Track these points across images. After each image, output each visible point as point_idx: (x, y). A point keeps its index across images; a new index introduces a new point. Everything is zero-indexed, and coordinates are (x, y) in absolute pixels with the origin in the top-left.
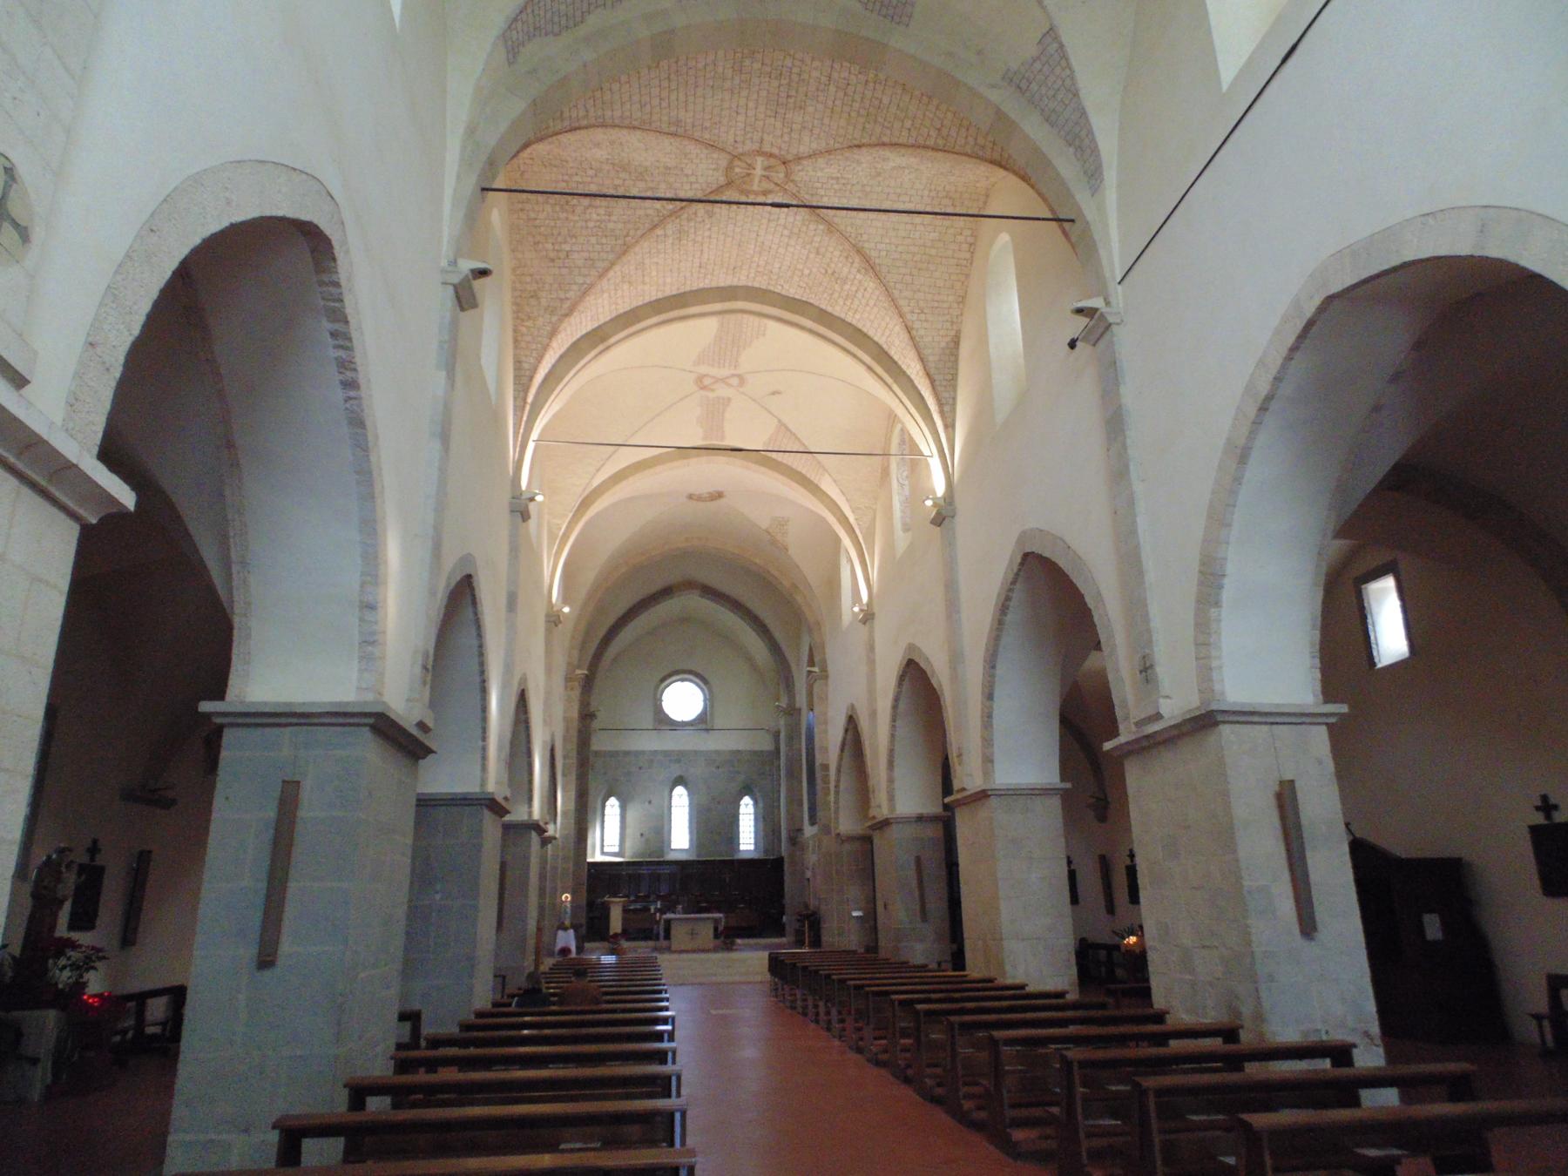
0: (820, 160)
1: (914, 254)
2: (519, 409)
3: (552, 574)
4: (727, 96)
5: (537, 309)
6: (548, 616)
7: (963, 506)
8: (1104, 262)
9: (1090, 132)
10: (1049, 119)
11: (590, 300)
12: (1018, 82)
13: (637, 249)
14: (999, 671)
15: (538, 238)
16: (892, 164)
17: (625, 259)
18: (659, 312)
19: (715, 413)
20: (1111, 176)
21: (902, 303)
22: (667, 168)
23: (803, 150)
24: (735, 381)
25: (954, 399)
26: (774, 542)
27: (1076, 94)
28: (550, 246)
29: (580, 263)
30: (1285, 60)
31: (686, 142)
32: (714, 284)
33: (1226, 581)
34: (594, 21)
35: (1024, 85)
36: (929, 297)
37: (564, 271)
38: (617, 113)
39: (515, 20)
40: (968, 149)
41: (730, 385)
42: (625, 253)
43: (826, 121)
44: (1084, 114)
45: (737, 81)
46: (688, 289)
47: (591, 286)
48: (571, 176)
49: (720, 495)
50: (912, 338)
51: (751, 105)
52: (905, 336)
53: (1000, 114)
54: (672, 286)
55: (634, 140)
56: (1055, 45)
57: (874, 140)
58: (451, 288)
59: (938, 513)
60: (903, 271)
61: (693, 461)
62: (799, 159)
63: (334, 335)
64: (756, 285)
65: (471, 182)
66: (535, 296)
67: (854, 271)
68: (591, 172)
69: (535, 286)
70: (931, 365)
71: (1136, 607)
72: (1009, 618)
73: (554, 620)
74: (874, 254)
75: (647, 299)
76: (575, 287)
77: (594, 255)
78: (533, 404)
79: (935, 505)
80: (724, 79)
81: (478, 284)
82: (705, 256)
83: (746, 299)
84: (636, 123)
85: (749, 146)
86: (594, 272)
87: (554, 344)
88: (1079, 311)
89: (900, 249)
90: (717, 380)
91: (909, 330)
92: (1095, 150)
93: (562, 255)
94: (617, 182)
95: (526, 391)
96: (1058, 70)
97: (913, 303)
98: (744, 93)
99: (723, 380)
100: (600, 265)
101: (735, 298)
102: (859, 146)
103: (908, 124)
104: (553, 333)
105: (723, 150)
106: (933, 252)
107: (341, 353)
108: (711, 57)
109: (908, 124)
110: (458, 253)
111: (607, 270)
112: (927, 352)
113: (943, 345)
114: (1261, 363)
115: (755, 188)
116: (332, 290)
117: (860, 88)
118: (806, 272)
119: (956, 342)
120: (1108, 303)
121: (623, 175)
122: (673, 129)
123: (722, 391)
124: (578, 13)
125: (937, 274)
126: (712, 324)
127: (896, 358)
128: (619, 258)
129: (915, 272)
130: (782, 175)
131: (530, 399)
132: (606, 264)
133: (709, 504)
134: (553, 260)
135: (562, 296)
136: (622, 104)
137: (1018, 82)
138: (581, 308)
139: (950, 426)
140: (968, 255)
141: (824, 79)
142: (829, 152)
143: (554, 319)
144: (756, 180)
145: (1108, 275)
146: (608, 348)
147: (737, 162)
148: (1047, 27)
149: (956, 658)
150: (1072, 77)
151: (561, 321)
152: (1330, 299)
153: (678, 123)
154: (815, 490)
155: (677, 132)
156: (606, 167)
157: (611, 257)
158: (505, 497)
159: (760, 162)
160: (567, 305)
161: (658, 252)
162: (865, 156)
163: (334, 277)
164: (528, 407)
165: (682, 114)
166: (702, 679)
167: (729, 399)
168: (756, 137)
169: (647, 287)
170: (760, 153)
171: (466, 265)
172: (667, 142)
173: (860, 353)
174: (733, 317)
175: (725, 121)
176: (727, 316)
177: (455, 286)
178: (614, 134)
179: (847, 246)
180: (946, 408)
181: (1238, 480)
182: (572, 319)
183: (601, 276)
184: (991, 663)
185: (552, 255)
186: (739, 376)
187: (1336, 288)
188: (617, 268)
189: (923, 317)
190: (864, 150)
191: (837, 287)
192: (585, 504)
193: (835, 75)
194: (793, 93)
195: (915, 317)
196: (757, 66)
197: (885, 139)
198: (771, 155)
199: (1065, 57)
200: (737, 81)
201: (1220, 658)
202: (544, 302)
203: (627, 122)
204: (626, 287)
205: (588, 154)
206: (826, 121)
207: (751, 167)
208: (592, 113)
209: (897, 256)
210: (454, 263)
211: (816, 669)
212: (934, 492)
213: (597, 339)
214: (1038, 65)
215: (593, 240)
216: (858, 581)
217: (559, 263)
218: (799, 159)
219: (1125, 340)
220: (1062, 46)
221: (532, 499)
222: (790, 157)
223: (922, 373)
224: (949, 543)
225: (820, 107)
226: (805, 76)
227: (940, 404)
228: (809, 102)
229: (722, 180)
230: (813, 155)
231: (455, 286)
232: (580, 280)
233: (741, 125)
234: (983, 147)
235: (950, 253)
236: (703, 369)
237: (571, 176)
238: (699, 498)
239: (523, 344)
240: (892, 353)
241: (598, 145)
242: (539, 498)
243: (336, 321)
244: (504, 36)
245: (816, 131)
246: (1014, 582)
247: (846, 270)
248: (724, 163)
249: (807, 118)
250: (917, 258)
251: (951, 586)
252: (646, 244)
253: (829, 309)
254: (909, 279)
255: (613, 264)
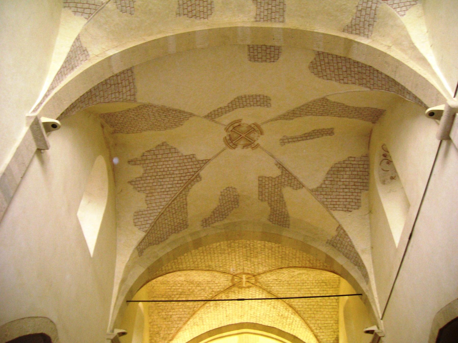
1: (314, 305)
4: (227, 255)
10: (347, 256)
11: (181, 333)
12: (332, 243)
13: (199, 312)
15: (160, 311)
17: (194, 316)
20: (372, 277)
21: (311, 325)
23: (260, 271)
27: (353, 247)
30: (410, 238)
31: (214, 272)
32: (234, 323)
35: (335, 244)
36: (323, 322)
37: (170, 323)
38: (184, 266)
39: (141, 242)
40: (321, 267)
42: (194, 314)
44: (357, 254)
45: (230, 250)
46: (223, 325)
47: (181, 328)
51: (237, 257)
53: (328, 257)
55: (193, 273)
56: (342, 231)
57: (286, 266)
60: (310, 312)
62: (259, 274)
64: (251, 322)
65: (122, 299)
66: (158, 333)
67: (290, 314)
68: (179, 285)
69: (158, 329)
74: (297, 307)
76: (174, 329)
77: (181, 316)
82: (228, 312)
84: (192, 268)
85: (239, 271)
86: (182, 323)
88: (368, 332)
89: (308, 304)
91: (316, 336)
92: (364, 267)
93: (169, 317)
94: (190, 288)
102: (281, 268)
103: (298, 260)
106: (321, 304)
109: (298, 260)
111: (187, 321)
115: (244, 286)
120: (378, 328)
121: (191, 285)
122: (207, 269)
124: (165, 237)
128: (192, 316)
129: (315, 312)
130: (254, 280)
132: (187, 319)
134: (165, 319)
135: (169, 332)
136: (186, 263)
137: (332, 243)
138: (177, 337)
141: (263, 247)
142: (271, 271)
144: (244, 283)
145: (377, 316)
148: (337, 226)
150: (350, 241)
153: (209, 266)
155: (209, 269)
157: (189, 316)
159: (244, 277)
160: (171, 336)
161: (208, 313)
162: (285, 271)
168: (241, 267)
169: (205, 326)
171: (117, 331)
172: (206, 273)
175: (228, 263)
178: (185, 272)
179: (285, 305)
183: (184, 324)
188: (191, 320)
189: (321, 330)
190: (284, 269)
191: (284, 321)
193: (267, 245)
197: (291, 265)
198: (248, 274)
199: (346, 235)
200: (230, 250)
202: (162, 335)
203: (189, 268)
205: (176, 280)
206: (267, 260)
207: (241, 278)
208: (174, 266)
209: (306, 307)
210: (113, 331)
214: (338, 238)
215: (181, 310)
217: (168, 320)
218: (259, 274)
220: (344, 231)
222: (255, 274)
225: (263, 256)
228: (259, 255)
229: (231, 284)
230: (264, 273)
232: (176, 326)
233: (234, 265)
234: (326, 266)
235: (329, 304)
237: (172, 287)
241: (180, 276)
244: (137, 248)
248: (230, 278)
249: (260, 260)
250: (315, 307)
252: (202, 310)
253: (283, 330)
255: (189, 319)
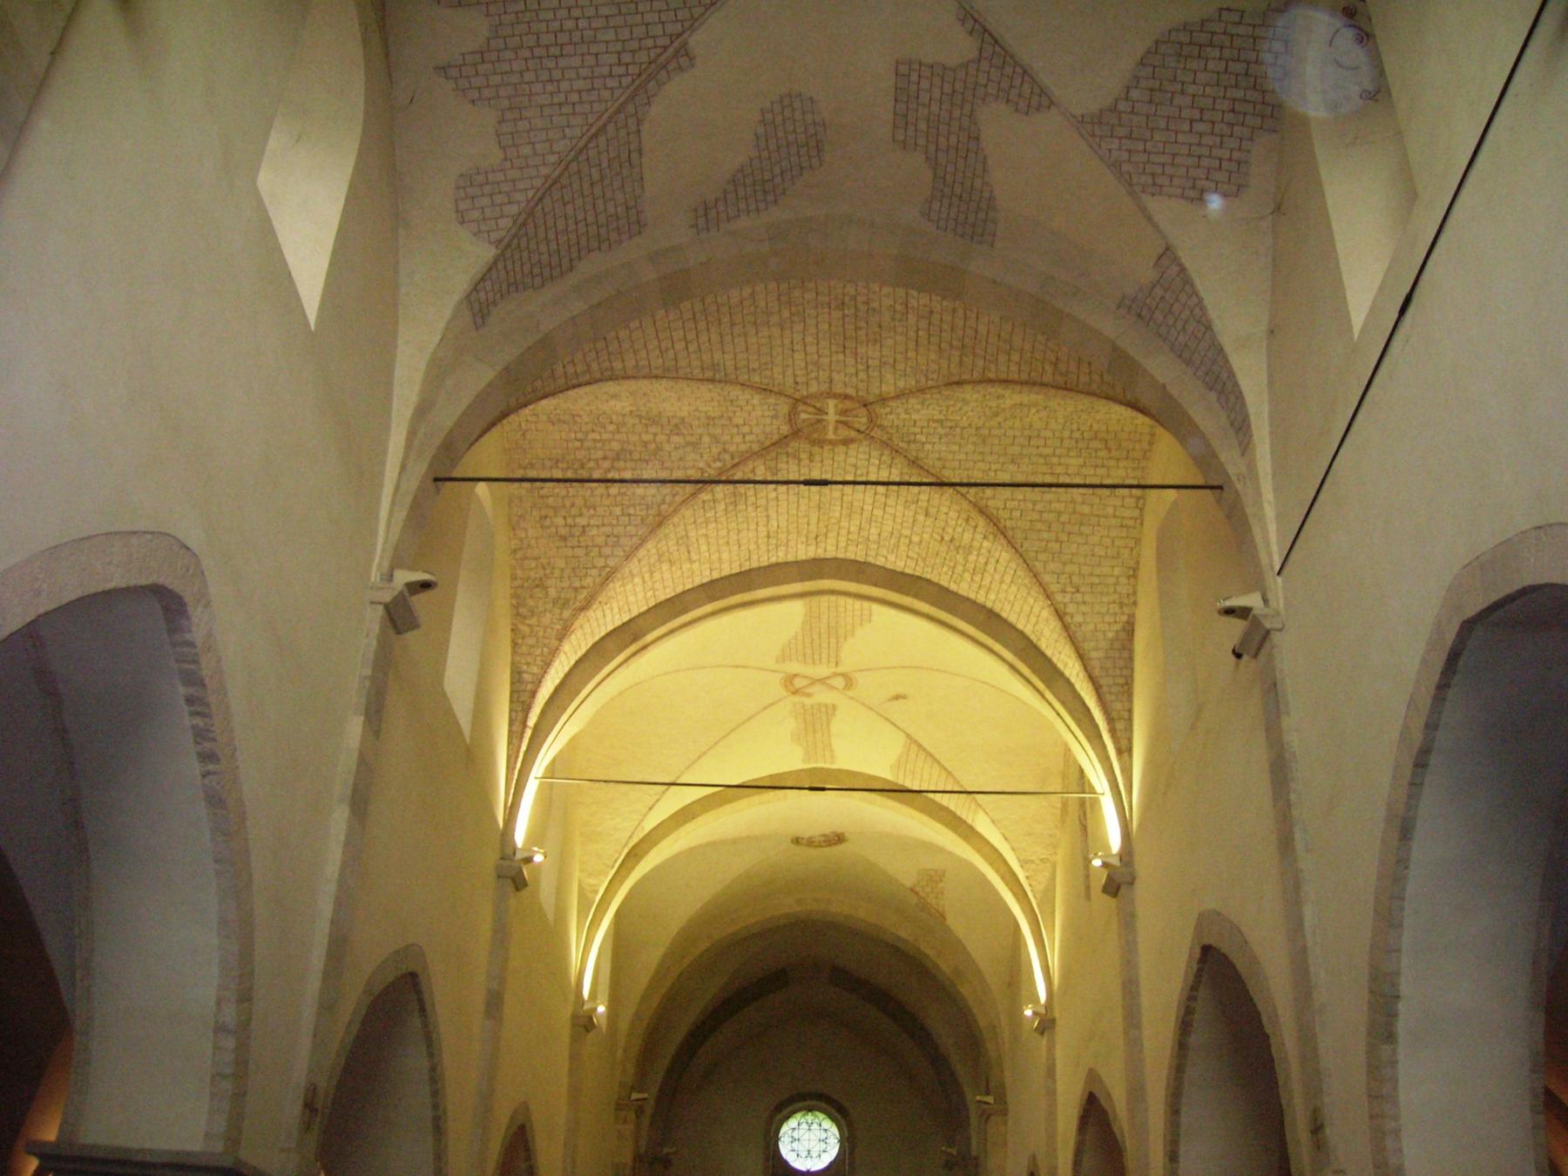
0: (912, 401)
2: (515, 736)
3: (587, 957)
5: (540, 606)
6: (575, 1017)
7: (1144, 865)
8: (1258, 540)
9: (1231, 374)
11: (615, 586)
12: (1139, 309)
14: (1185, 1118)
16: (1009, 402)
17: (662, 532)
18: (712, 599)
19: (815, 723)
21: (1047, 578)
22: (709, 418)
23: (888, 389)
24: (839, 682)
25: (1130, 711)
26: (924, 906)
28: (560, 521)
29: (600, 540)
30: (1403, 310)
31: (729, 388)
32: (791, 558)
33: (1401, 1006)
34: (586, 268)
39: (482, 279)
41: (833, 688)
42: (660, 524)
43: (911, 354)
46: (755, 565)
48: (587, 434)
49: (839, 839)
50: (1066, 627)
52: (1054, 623)
54: (729, 564)
56: (1175, 269)
58: (381, 608)
59: (1109, 878)
60: (1045, 535)
61: (743, 803)
62: (883, 400)
63: (190, 700)
65: (419, 469)
66: (541, 584)
67: (979, 537)
68: (611, 428)
70: (1095, 664)
71: (1307, 1037)
72: (1193, 1040)
73: (584, 1023)
75: (698, 582)
76: (594, 572)
78: (536, 728)
79: (1105, 865)
80: (769, 314)
81: (419, 601)
83: (834, 577)
87: (566, 647)
88: (1229, 612)
90: (814, 681)
91: (1060, 615)
92: (1240, 397)
93: (577, 531)
94: (646, 437)
95: (527, 710)
96: (1183, 298)
97: (1063, 579)
98: (798, 327)
99: (822, 681)
100: (627, 543)
101: (821, 576)
102: (959, 383)
103: (1015, 357)
104: (562, 636)
105: (780, 393)
107: (198, 721)
108: (747, 291)
109: (1015, 357)
110: (397, 562)
112: (1087, 646)
113: (1110, 635)
114: (1412, 704)
115: (831, 436)
116: (186, 650)
117: (947, 318)
118: (916, 539)
119: (1129, 629)
120: (1265, 601)
121: (653, 429)
122: (708, 374)
123: (822, 696)
125: (1095, 539)
126: (796, 608)
127: (1049, 653)
129: (1064, 537)
130: (864, 420)
131: (532, 721)
133: (827, 850)
134: (564, 539)
135: (577, 584)
137: (1139, 309)
139: (1125, 751)
140: (1136, 513)
142: (922, 391)
143: (567, 614)
144: (831, 428)
146: (644, 648)
147: (801, 407)
149: (1137, 1093)
151: (574, 616)
152: (1468, 626)
153: (715, 367)
154: (967, 832)
155: (714, 377)
156: (630, 421)
158: (491, 858)
160: (583, 595)
161: (707, 522)
163: (188, 636)
164: (528, 733)
165: (718, 356)
166: (838, 1111)
167: (834, 707)
168: (823, 375)
169: (695, 566)
170: (830, 395)
171: (403, 577)
172: (704, 390)
173: (997, 647)
174: (824, 599)
176: (816, 599)
177: (387, 607)
178: (632, 385)
179: (965, 505)
180: (1120, 725)
181: (1403, 862)
182: (590, 613)
183: (628, 557)
184: (1174, 1110)
185: (563, 531)
186: (844, 675)
187: (1470, 612)
188: (650, 545)
189: (1079, 597)
191: (960, 558)
192: (635, 854)
193: (913, 303)
194: (863, 324)
195: (1067, 598)
196: (810, 296)
197: (992, 375)
198: (846, 397)
199: (1188, 281)
200: (786, 314)
201: (1396, 1118)
202: (553, 593)
204: (665, 567)
206: (911, 354)
207: (821, 411)
208: (595, 366)
209: (1035, 516)
210: (390, 577)
211: (990, 1099)
212: (1106, 847)
213: (629, 636)
215: (618, 511)
216: (1043, 967)
218: (883, 400)
219: (1288, 651)
220: (1183, 269)
221: (529, 860)
222: (871, 398)
223: (1082, 674)
224: (1128, 922)
226: (875, 305)
227: (1110, 720)
229: (785, 429)
231: (387, 607)
232: (600, 562)
236: (794, 667)
238: (810, 843)
239: (524, 649)
240: (1043, 645)
241: (614, 396)
242: (538, 858)
243: (194, 684)
245: (901, 366)
246: (1194, 988)
247: (967, 536)
248: (784, 408)
250: (1064, 518)
251: (1130, 987)
253: (953, 587)
254: (1056, 546)
255: (643, 541)
